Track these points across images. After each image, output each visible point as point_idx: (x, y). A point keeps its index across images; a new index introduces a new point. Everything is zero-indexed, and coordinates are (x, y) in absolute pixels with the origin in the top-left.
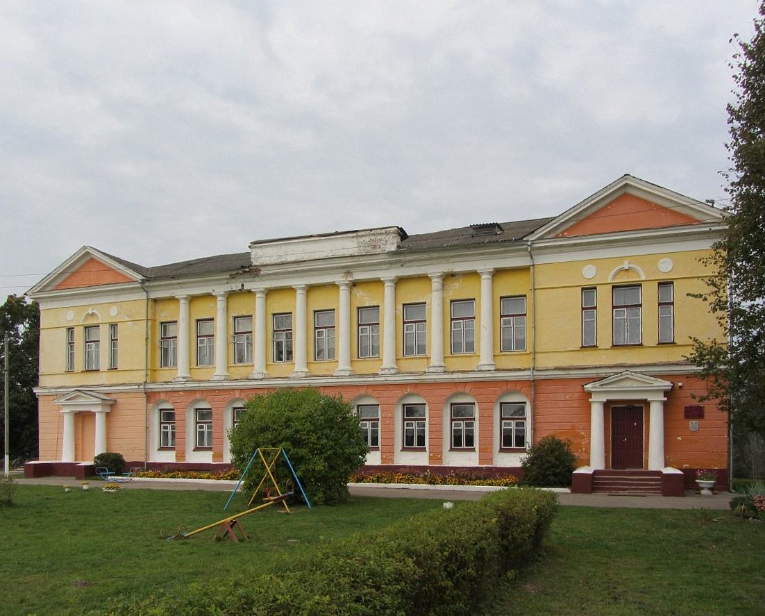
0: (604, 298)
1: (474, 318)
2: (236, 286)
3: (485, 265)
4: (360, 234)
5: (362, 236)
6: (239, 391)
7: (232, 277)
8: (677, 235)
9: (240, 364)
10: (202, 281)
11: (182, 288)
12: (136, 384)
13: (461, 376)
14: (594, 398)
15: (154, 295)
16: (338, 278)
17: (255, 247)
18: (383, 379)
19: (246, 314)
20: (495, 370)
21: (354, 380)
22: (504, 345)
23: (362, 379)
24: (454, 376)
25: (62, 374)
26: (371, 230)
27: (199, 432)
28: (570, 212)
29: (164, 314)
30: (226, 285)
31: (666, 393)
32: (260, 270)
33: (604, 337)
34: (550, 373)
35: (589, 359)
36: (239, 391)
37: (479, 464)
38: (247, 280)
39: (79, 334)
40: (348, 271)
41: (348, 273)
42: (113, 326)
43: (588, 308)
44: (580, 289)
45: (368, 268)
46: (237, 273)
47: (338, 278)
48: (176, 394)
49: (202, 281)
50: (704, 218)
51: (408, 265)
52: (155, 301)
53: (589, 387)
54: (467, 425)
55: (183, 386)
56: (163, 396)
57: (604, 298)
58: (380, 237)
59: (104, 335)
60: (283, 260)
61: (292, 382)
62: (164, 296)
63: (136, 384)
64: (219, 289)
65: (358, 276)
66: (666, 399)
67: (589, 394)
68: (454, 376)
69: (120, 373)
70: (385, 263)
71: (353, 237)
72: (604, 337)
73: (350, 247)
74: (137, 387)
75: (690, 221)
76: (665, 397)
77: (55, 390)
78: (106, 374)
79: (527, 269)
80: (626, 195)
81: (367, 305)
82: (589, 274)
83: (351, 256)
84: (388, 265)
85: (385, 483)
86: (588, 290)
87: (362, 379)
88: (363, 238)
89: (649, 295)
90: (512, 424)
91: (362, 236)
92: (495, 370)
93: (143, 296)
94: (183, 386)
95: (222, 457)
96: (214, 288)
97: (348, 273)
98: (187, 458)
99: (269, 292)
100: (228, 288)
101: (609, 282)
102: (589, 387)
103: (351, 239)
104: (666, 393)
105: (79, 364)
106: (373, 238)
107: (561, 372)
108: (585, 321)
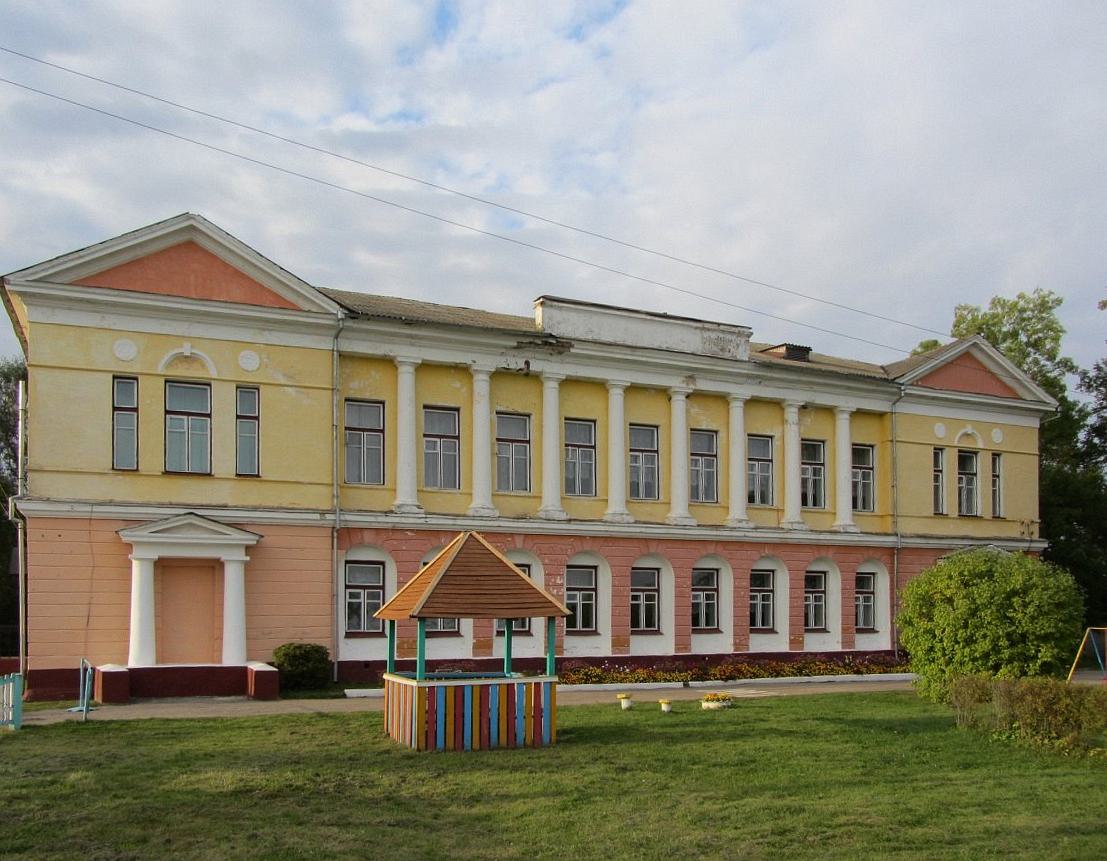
0: (151, 398)
1: (346, 428)
2: (516, 362)
3: (847, 403)
4: (707, 326)
5: (709, 330)
6: (522, 537)
7: (519, 347)
8: (961, 401)
9: (763, 506)
10: (457, 341)
11: (412, 345)
12: (315, 511)
13: (828, 537)
14: (137, 552)
15: (348, 346)
16: (675, 382)
17: (552, 306)
18: (742, 534)
19: (521, 411)
20: (636, 522)
21: (704, 532)
22: (861, 500)
23: (715, 533)
24: (821, 537)
25: (931, 517)
26: (719, 324)
27: (349, 603)
28: (113, 243)
29: (367, 383)
30: (499, 358)
31: (248, 549)
32: (572, 346)
33: (152, 459)
34: (912, 540)
35: (122, 489)
36: (522, 537)
37: (474, 655)
38: (537, 355)
39: (949, 461)
40: (691, 375)
41: (691, 378)
42: (996, 456)
43: (124, 410)
44: (111, 376)
45: (718, 377)
46: (531, 343)
47: (675, 382)
48: (398, 536)
49: (457, 341)
50: (307, 307)
51: (767, 383)
52: (343, 356)
53: (127, 536)
54: (708, 597)
55: (422, 521)
56: (368, 537)
57: (151, 398)
58: (729, 337)
59: (982, 465)
60: (595, 337)
61: (616, 529)
62: (370, 352)
63: (315, 511)
64: (485, 362)
65: (704, 385)
66: (248, 558)
67: (129, 546)
68: (821, 537)
69: (217, 482)
70: (748, 376)
71: (696, 328)
72: (152, 459)
73: (691, 341)
74: (317, 516)
75: (286, 306)
76: (247, 555)
77: (89, 509)
78: (228, 485)
79: (881, 415)
80: (190, 245)
81: (704, 427)
82: (126, 354)
83: (692, 354)
84: (745, 379)
85: (808, 675)
86: (124, 381)
87: (715, 533)
88: (710, 333)
89: (223, 403)
90: (362, 595)
91: (709, 330)
92: (862, 533)
93: (327, 344)
94: (422, 521)
95: (490, 646)
96: (474, 357)
97: (691, 378)
98: (494, 653)
99: (568, 383)
100: (501, 362)
101: (956, 444)
102: (127, 536)
103: (694, 331)
104: (248, 549)
105: (949, 504)
106: (721, 335)
107: (919, 541)
108: (192, 434)
